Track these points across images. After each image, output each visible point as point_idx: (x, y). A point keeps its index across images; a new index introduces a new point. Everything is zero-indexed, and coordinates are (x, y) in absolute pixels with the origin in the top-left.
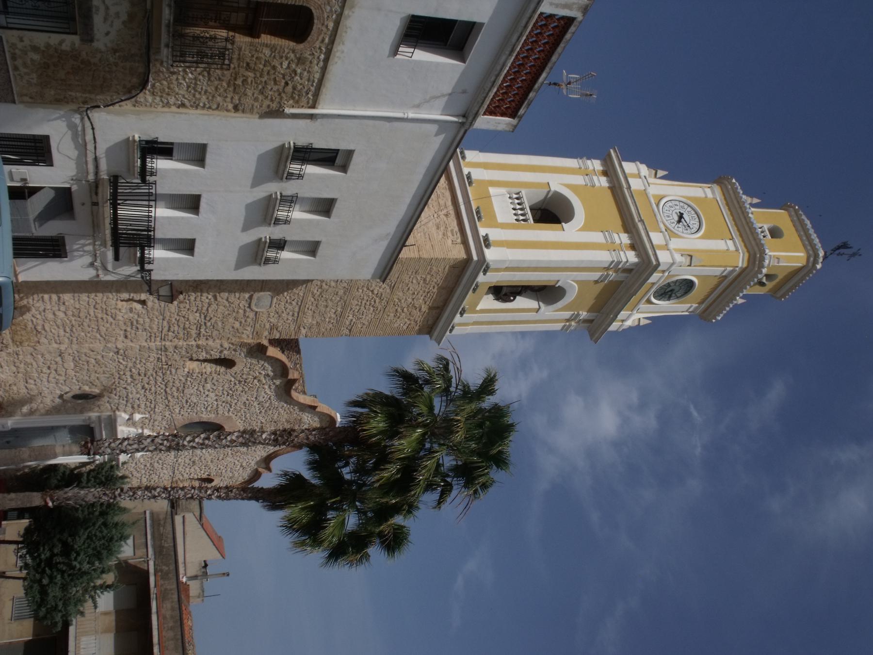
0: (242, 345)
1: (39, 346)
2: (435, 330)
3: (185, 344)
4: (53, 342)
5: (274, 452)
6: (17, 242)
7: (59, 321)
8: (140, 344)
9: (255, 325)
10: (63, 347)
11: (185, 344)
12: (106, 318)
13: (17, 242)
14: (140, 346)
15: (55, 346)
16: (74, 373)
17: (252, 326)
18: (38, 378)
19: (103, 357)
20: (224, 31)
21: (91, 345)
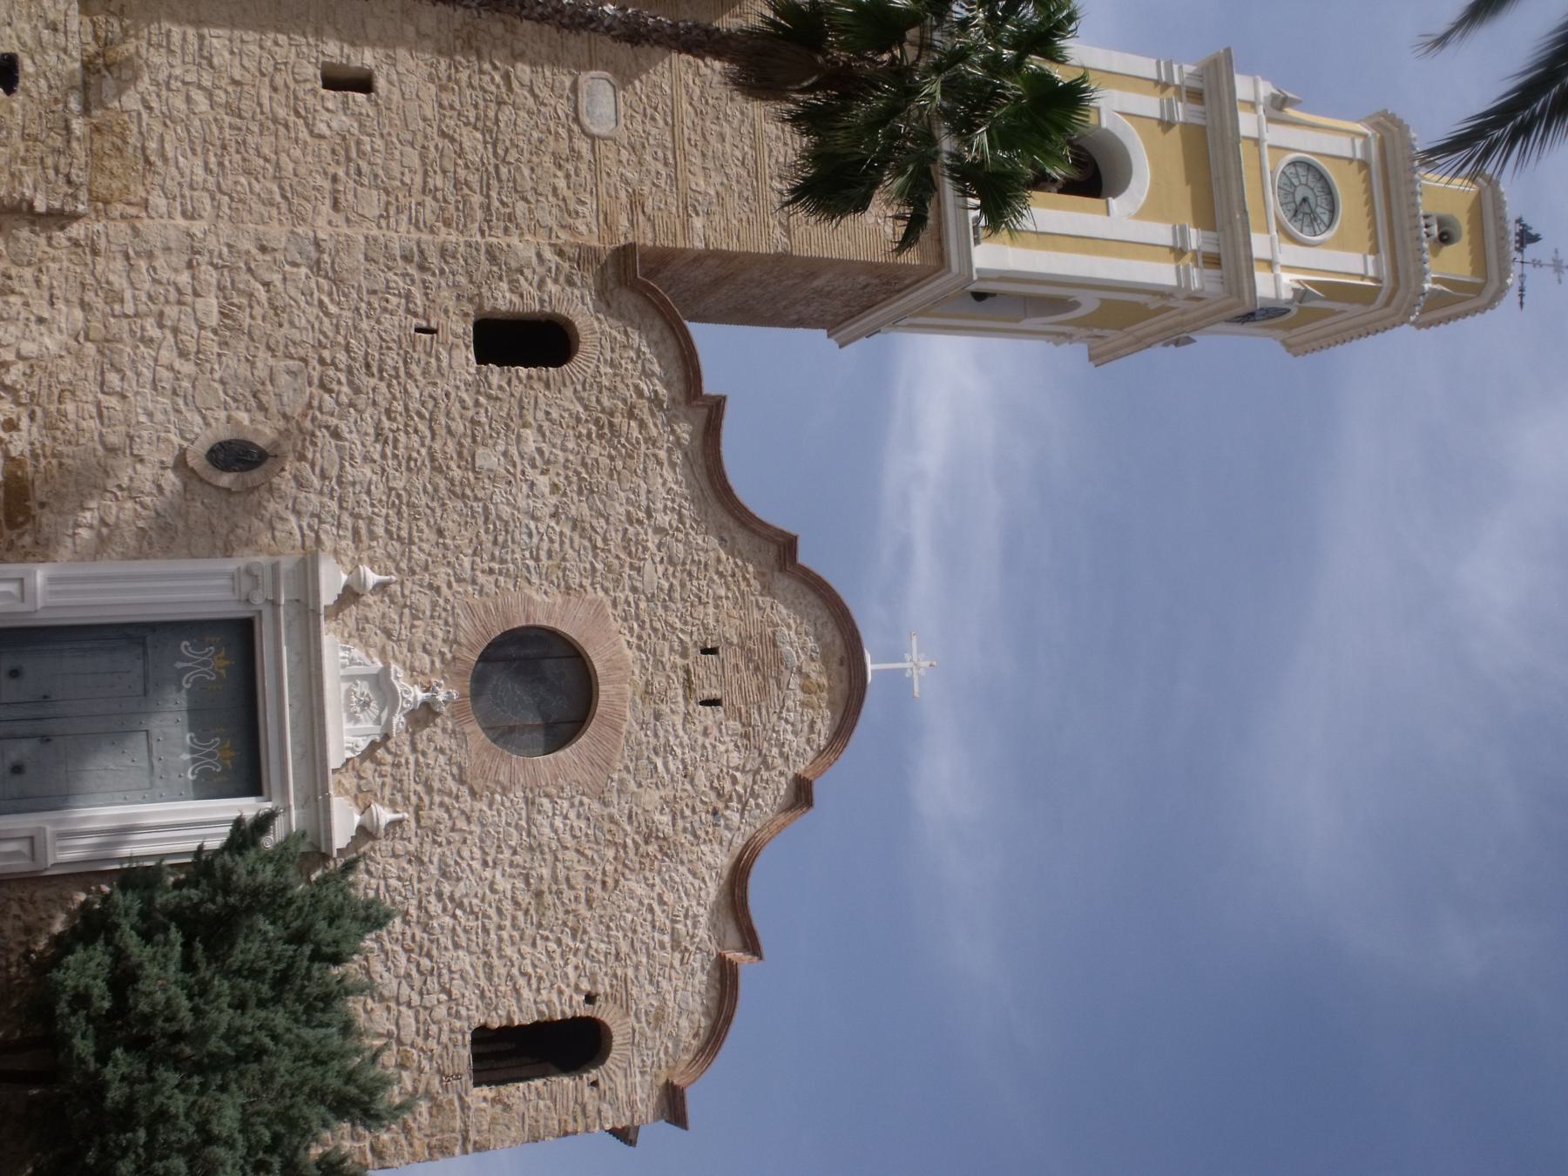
0: (585, 257)
1: (146, 221)
2: (948, 240)
3: (462, 239)
4: (267, 83)
5: (746, 846)
6: (59, 588)
7: (197, 123)
8: (366, 232)
9: (596, 186)
10: (198, 227)
11: (462, 239)
12: (295, 123)
13: (59, 588)
14: (366, 238)
15: (181, 221)
16: (216, 349)
17: (592, 192)
18: (394, 398)
19: (285, 279)
20: (220, 32)
21: (261, 228)
